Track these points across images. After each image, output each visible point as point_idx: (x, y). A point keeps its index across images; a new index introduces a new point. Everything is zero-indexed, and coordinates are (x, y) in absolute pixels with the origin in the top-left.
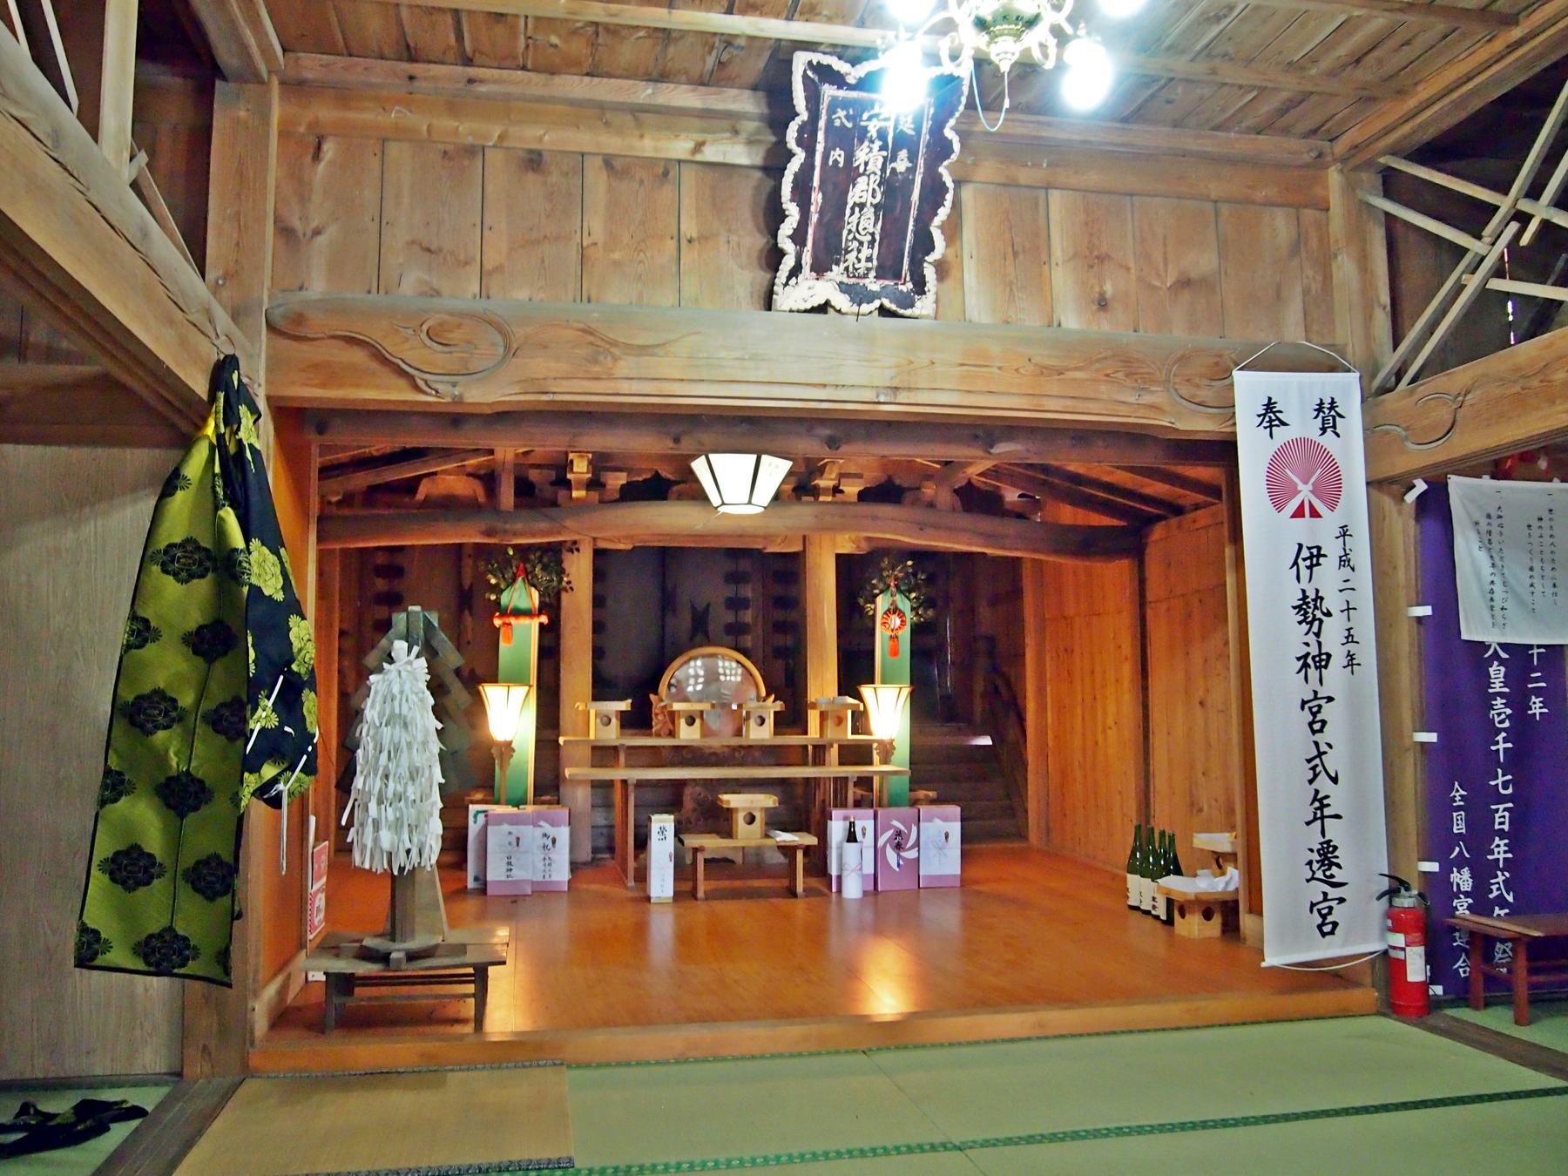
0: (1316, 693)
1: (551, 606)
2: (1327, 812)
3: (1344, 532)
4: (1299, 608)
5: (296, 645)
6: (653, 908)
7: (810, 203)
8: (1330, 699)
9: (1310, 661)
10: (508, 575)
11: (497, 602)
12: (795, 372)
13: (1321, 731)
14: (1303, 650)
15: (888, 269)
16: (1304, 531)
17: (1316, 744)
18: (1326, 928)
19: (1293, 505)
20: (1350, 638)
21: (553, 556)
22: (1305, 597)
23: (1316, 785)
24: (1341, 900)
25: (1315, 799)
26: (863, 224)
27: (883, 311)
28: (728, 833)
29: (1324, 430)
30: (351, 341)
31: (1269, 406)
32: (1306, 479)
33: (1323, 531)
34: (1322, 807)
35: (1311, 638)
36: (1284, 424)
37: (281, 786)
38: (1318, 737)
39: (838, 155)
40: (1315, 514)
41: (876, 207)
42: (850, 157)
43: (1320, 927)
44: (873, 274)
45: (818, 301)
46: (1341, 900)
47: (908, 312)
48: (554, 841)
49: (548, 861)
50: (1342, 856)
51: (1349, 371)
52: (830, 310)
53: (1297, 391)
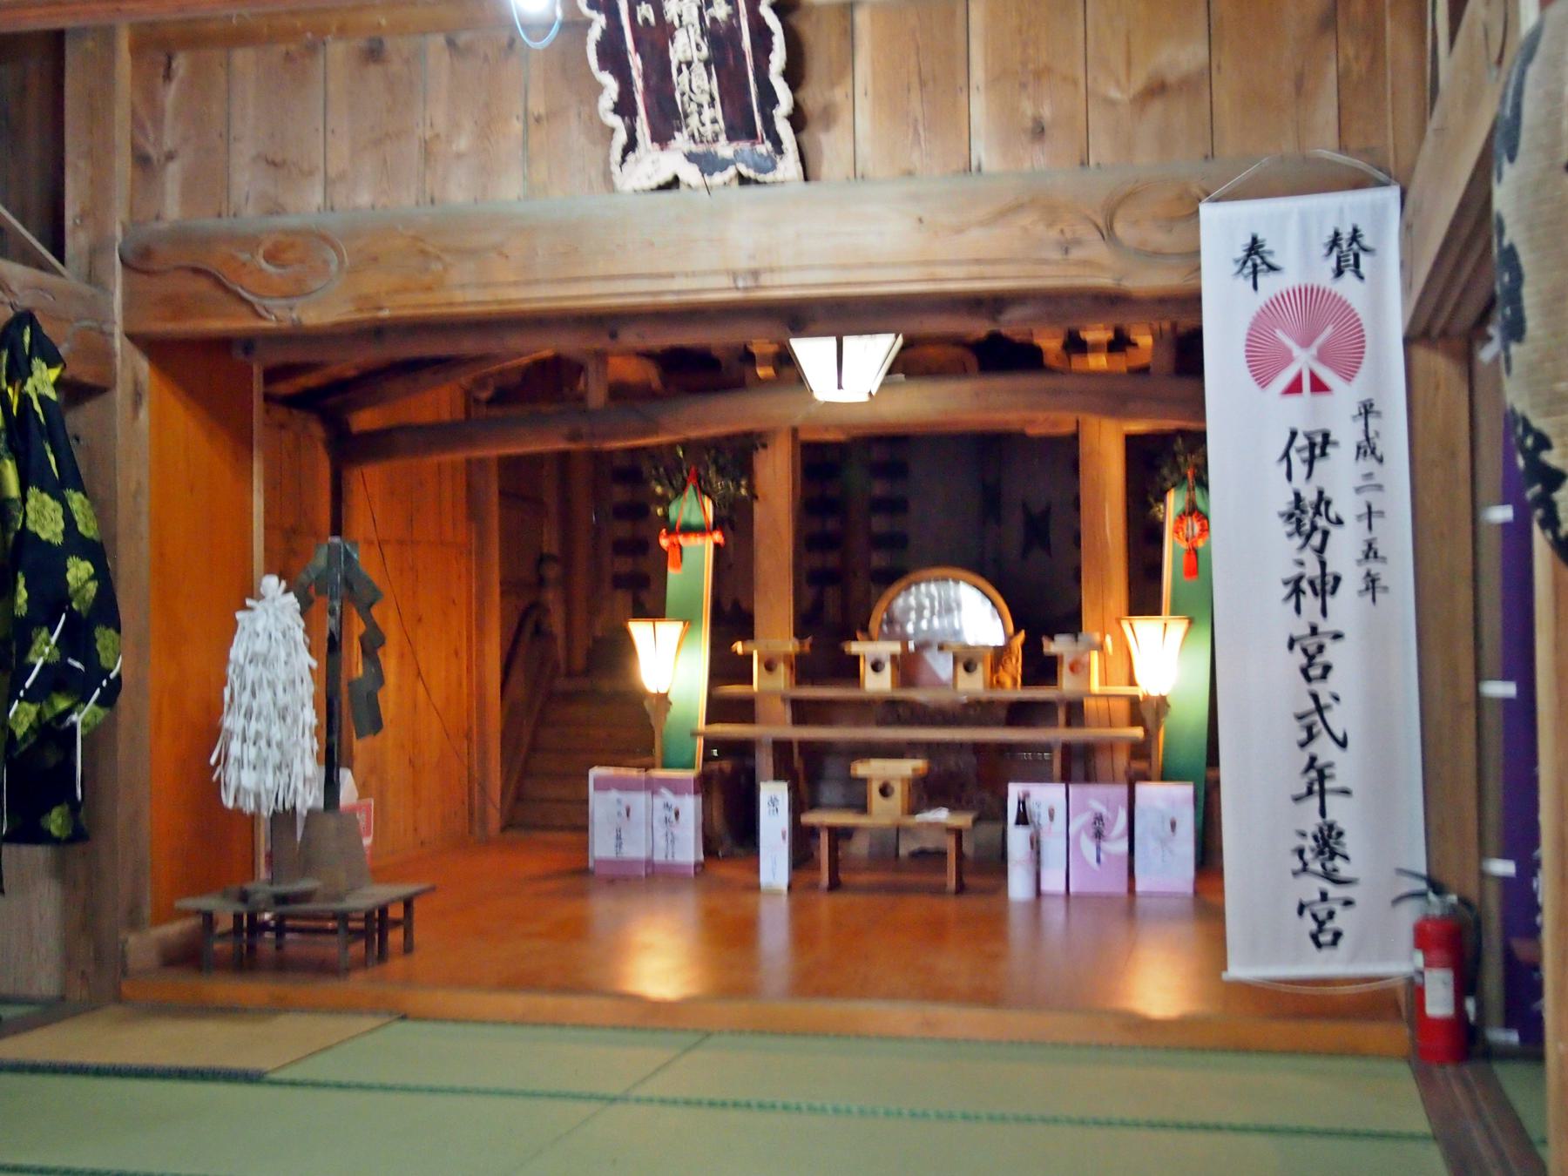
0: (1314, 631)
1: (734, 521)
3: (1367, 410)
4: (1290, 516)
7: (629, 68)
8: (1337, 636)
9: (1305, 585)
10: (677, 482)
11: (666, 516)
12: (471, 295)
13: (1324, 676)
14: (1295, 571)
15: (740, 128)
16: (1301, 413)
17: (1315, 697)
18: (1324, 936)
19: (1286, 378)
20: (1370, 552)
21: (737, 455)
23: (1314, 748)
24: (1348, 903)
26: (696, 85)
27: (743, 180)
28: (862, 807)
29: (1339, 272)
30: (197, 271)
31: (1255, 247)
33: (1337, 412)
35: (1309, 557)
37: (75, 717)
38: (1317, 687)
39: (646, 11)
40: (1318, 386)
41: (707, 64)
42: (659, 12)
44: (723, 137)
45: (665, 176)
46: (1348, 903)
47: (769, 177)
48: (677, 814)
49: (671, 839)
50: (1350, 844)
51: (1380, 184)
52: (682, 187)
53: (1296, 225)
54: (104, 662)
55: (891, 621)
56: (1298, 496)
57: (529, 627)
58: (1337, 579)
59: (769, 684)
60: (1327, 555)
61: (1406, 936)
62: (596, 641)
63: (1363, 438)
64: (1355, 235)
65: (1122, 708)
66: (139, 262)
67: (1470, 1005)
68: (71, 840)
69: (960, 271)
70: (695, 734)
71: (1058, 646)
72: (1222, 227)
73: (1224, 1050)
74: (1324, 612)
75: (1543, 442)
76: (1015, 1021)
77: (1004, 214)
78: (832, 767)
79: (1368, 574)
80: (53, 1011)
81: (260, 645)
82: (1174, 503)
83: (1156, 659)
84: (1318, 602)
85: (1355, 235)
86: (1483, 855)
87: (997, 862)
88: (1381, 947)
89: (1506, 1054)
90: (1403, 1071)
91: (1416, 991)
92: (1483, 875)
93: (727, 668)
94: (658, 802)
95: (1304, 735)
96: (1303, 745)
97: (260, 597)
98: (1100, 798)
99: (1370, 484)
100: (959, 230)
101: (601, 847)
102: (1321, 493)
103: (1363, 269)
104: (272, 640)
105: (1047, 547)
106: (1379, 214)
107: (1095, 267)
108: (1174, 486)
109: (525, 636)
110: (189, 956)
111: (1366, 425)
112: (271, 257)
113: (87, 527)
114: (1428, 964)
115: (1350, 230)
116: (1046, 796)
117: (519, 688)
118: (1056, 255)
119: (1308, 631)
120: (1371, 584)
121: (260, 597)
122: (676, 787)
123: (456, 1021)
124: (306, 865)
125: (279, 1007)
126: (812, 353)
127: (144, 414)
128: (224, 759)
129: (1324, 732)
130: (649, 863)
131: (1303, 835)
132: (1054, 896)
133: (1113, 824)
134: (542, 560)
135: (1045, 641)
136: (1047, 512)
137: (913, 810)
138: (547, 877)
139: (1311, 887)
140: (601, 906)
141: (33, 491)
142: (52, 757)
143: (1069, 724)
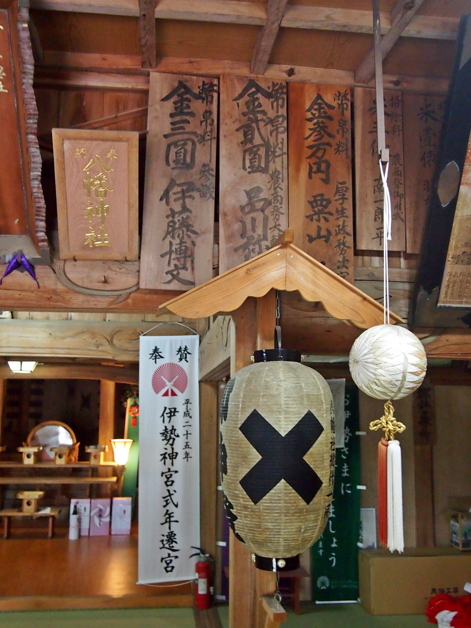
0: (169, 469)
8: (176, 472)
9: (167, 456)
13: (171, 485)
14: (165, 451)
16: (167, 402)
18: (169, 568)
19: (164, 391)
20: (187, 446)
23: (167, 508)
24: (176, 557)
25: (166, 514)
29: (181, 359)
31: (156, 350)
33: (179, 402)
34: (170, 517)
35: (169, 447)
38: (169, 488)
40: (173, 394)
43: (166, 568)
46: (176, 557)
50: (178, 538)
53: (168, 344)
55: (34, 438)
56: (166, 427)
58: (177, 454)
60: (174, 447)
61: (193, 568)
63: (186, 411)
65: (110, 470)
67: (212, 589)
69: (63, 351)
71: (90, 450)
72: (146, 343)
73: (136, 608)
74: (172, 464)
75: (231, 506)
78: (9, 495)
79: (186, 453)
82: (130, 402)
83: (121, 453)
84: (171, 461)
85: (186, 349)
86: (217, 540)
88: (186, 571)
90: (189, 613)
91: (195, 585)
92: (217, 546)
95: (165, 503)
96: (164, 506)
98: (102, 503)
99: (188, 425)
102: (173, 427)
103: (188, 359)
107: (105, 352)
108: (130, 397)
111: (187, 407)
114: (200, 577)
115: (184, 347)
116: (84, 504)
118: (94, 348)
119: (167, 470)
120: (187, 455)
126: (11, 363)
129: (171, 503)
131: (163, 536)
132: (85, 536)
133: (105, 511)
135: (86, 447)
137: (38, 510)
139: (165, 552)
143: (93, 476)
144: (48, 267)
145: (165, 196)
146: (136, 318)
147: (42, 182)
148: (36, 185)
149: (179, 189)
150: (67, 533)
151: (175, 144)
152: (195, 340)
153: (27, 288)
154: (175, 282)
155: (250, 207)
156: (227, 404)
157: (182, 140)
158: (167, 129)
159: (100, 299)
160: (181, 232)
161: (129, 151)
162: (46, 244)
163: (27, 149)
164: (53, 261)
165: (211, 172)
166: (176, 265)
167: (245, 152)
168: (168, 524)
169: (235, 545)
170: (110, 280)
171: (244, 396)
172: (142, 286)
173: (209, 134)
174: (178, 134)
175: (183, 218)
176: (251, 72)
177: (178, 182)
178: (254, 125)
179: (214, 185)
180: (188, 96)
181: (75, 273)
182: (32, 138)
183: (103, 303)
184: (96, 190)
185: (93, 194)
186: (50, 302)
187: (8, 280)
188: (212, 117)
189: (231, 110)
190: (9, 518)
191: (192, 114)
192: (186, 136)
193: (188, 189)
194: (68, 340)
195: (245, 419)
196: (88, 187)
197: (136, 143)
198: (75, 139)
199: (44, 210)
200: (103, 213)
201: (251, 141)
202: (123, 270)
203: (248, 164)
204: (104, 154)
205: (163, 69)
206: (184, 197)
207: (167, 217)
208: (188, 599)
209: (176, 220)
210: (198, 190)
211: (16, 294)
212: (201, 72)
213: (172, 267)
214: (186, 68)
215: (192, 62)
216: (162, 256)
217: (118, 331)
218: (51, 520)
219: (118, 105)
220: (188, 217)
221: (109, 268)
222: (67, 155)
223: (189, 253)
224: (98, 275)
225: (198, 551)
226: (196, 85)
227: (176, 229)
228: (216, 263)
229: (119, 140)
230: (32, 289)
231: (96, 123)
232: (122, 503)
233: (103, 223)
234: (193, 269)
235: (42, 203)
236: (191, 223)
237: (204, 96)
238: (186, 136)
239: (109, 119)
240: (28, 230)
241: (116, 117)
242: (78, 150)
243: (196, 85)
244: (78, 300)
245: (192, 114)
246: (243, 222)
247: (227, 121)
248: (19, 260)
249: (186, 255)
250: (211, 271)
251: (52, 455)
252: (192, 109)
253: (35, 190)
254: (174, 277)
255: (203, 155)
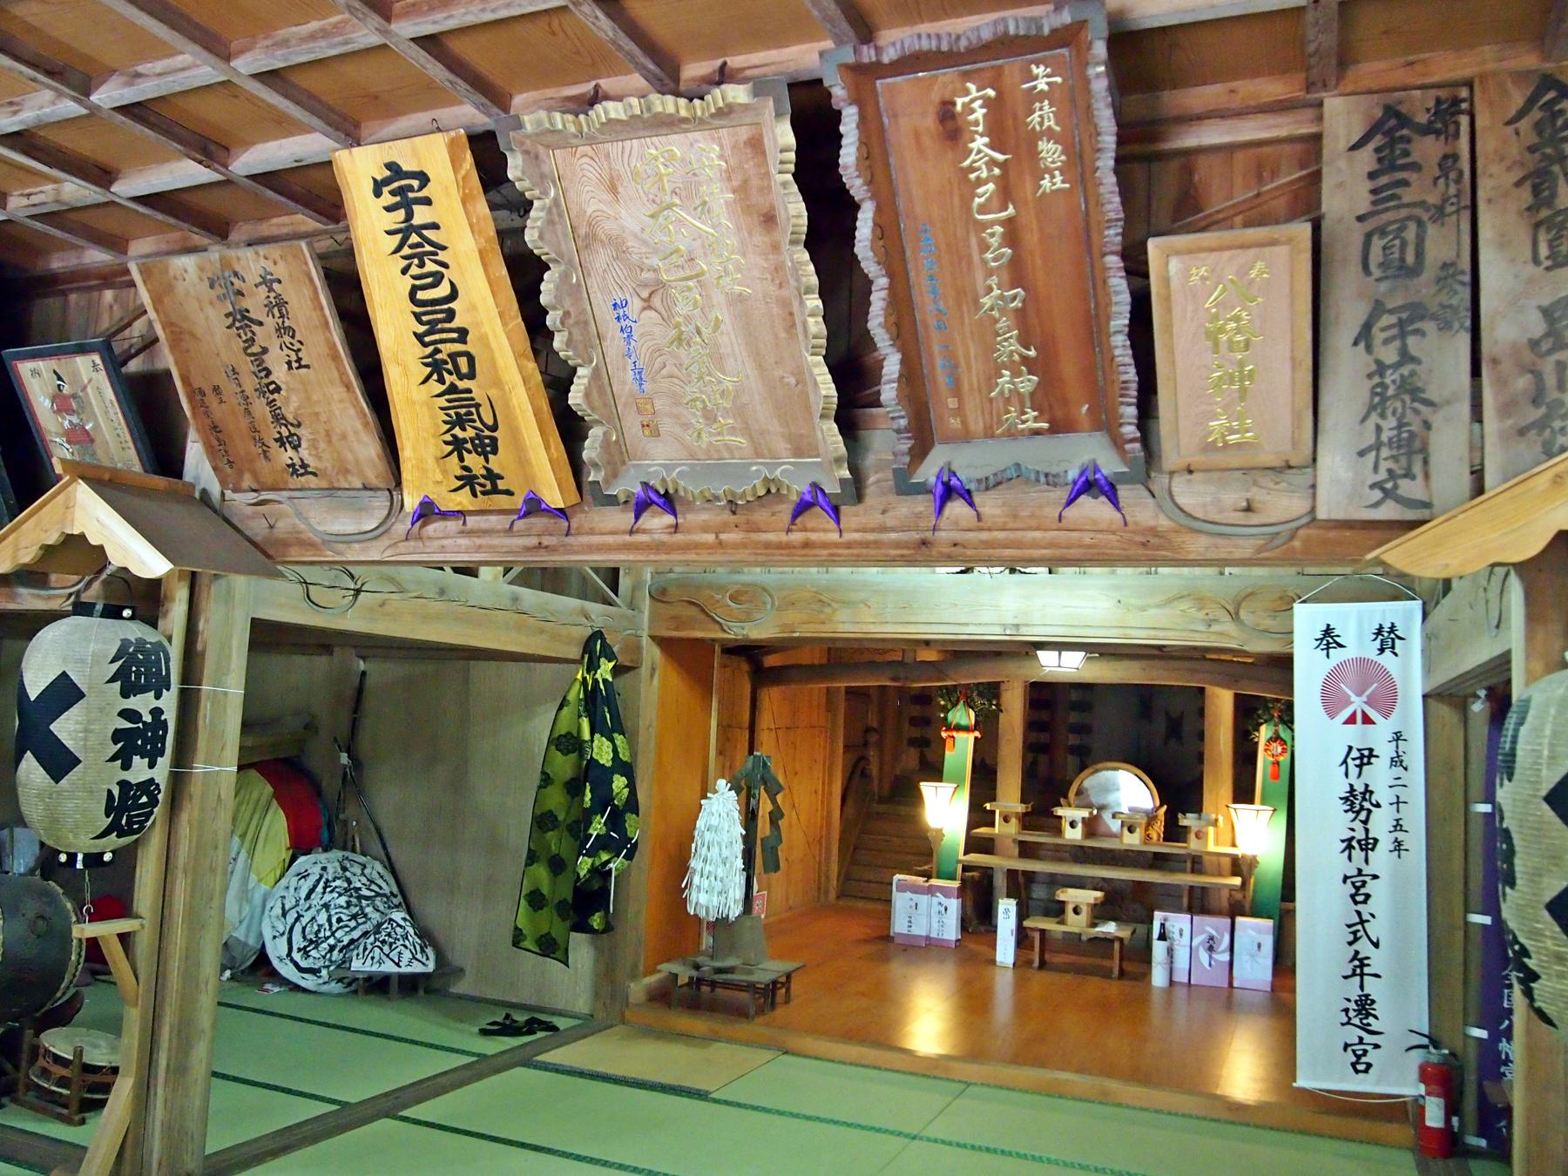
0: (1360, 871)
1: (987, 726)
2: (1366, 970)
3: (1398, 737)
4: (1346, 799)
5: (616, 790)
6: (998, 971)
8: (1375, 877)
9: (1354, 843)
11: (946, 719)
12: (848, 628)
13: (1365, 902)
16: (1355, 736)
17: (1359, 913)
18: (1360, 1065)
19: (1346, 713)
20: (1398, 826)
22: (1352, 789)
23: (1356, 946)
24: (1377, 1046)
25: (1355, 958)
29: (1382, 650)
31: (1328, 631)
32: (1363, 693)
33: (1379, 736)
34: (1362, 966)
35: (1358, 825)
36: (1341, 646)
38: (1360, 907)
40: (1367, 720)
43: (1354, 1065)
46: (1377, 1046)
49: (942, 924)
50: (1379, 1009)
53: (1356, 621)
54: (629, 834)
55: (1079, 793)
57: (858, 772)
58: (1376, 840)
59: (1004, 830)
62: (897, 778)
64: (1392, 629)
65: (1226, 862)
66: (659, 596)
68: (604, 931)
69: (1143, 633)
70: (959, 861)
72: (1308, 619)
73: (1293, 1131)
74: (1367, 861)
75: (1524, 952)
76: (1161, 1097)
77: (1169, 601)
80: (589, 1027)
81: (714, 821)
82: (1265, 732)
83: (1252, 833)
85: (1392, 629)
87: (1143, 954)
88: (1397, 1076)
89: (1477, 1153)
90: (1408, 1159)
92: (1466, 1036)
93: (979, 815)
94: (935, 900)
95: (1351, 938)
96: (1350, 944)
97: (716, 792)
98: (1212, 925)
99: (1398, 784)
100: (1143, 609)
101: (899, 926)
104: (720, 817)
105: (1179, 738)
106: (1409, 613)
107: (1226, 635)
109: (856, 774)
110: (663, 996)
112: (732, 598)
113: (624, 756)
114: (1428, 1094)
116: (1179, 923)
117: (850, 810)
118: (1202, 628)
119: (1355, 872)
120: (1398, 846)
121: (716, 792)
122: (946, 892)
123: (816, 1058)
124: (732, 949)
125: (715, 1038)
127: (656, 681)
128: (690, 884)
130: (928, 938)
134: (868, 730)
135: (1180, 816)
136: (1181, 717)
137: (1094, 925)
138: (866, 941)
139: (1353, 1034)
140: (896, 968)
141: (597, 736)
142: (596, 885)
143: (1193, 871)
144: (1139, 486)
145: (1364, 336)
146: (1286, 574)
147: (1131, 336)
148: (1120, 344)
149: (1393, 319)
150: (1146, 974)
151: (1382, 232)
152: (1411, 611)
153: (1103, 526)
154: (1390, 503)
155: (1551, 340)
156: (1513, 749)
157: (1395, 222)
158: (1364, 204)
159: (1241, 542)
160: (1398, 404)
161: (1292, 260)
162: (1137, 445)
163: (1105, 282)
164: (1149, 476)
165: (1460, 278)
166: (1390, 471)
167: (1537, 226)
168: (1357, 979)
169: (1528, 1032)
170: (1255, 505)
171: (1555, 734)
172: (1322, 514)
173: (1454, 200)
174: (1387, 209)
175: (1402, 376)
176: (1546, 59)
177: (1390, 306)
178: (1556, 168)
179: (1467, 303)
180: (1405, 132)
181: (1190, 495)
182: (1114, 261)
183: (1245, 549)
184: (1230, 341)
185: (1223, 348)
186: (1147, 550)
187: (1072, 513)
188: (1458, 165)
189: (1500, 144)
190: (1043, 932)
191: (1415, 167)
192: (1404, 213)
193: (1411, 318)
194: (1152, 611)
195: (1557, 779)
196: (1212, 336)
197: (1307, 244)
198: (1190, 252)
199: (1135, 386)
200: (1242, 380)
201: (1549, 202)
202: (1283, 485)
203: (1544, 251)
204: (1243, 272)
205: (1350, 88)
206: (1403, 335)
207: (1370, 376)
208: (1402, 1132)
209: (1388, 381)
210: (1434, 317)
211: (1087, 538)
212: (1428, 80)
213: (1382, 475)
214: (1399, 77)
215: (1411, 64)
216: (1362, 454)
217: (1251, 594)
218: (1117, 945)
219: (1260, 172)
220: (1413, 374)
221: (1255, 483)
222: (1175, 284)
223: (1417, 444)
224: (1233, 497)
225: (1425, 1041)
226: (1420, 107)
227: (1389, 398)
228: (1477, 461)
229: (1273, 243)
230: (1114, 527)
231: (1218, 212)
232: (1255, 932)
233: (1242, 399)
234: (1427, 476)
235: (1131, 374)
236: (1419, 384)
237: (1439, 125)
238: (1404, 213)
239: (1244, 201)
240: (1106, 423)
241: (1258, 195)
242: (1194, 271)
243: (1420, 107)
244: (1198, 545)
245: (1415, 167)
246: (1538, 375)
247: (1494, 169)
248: (1091, 478)
249: (1412, 449)
250: (1466, 480)
251: (1115, 825)
252: (1415, 157)
253: (1117, 352)
254: (1387, 494)
255: (1443, 244)
